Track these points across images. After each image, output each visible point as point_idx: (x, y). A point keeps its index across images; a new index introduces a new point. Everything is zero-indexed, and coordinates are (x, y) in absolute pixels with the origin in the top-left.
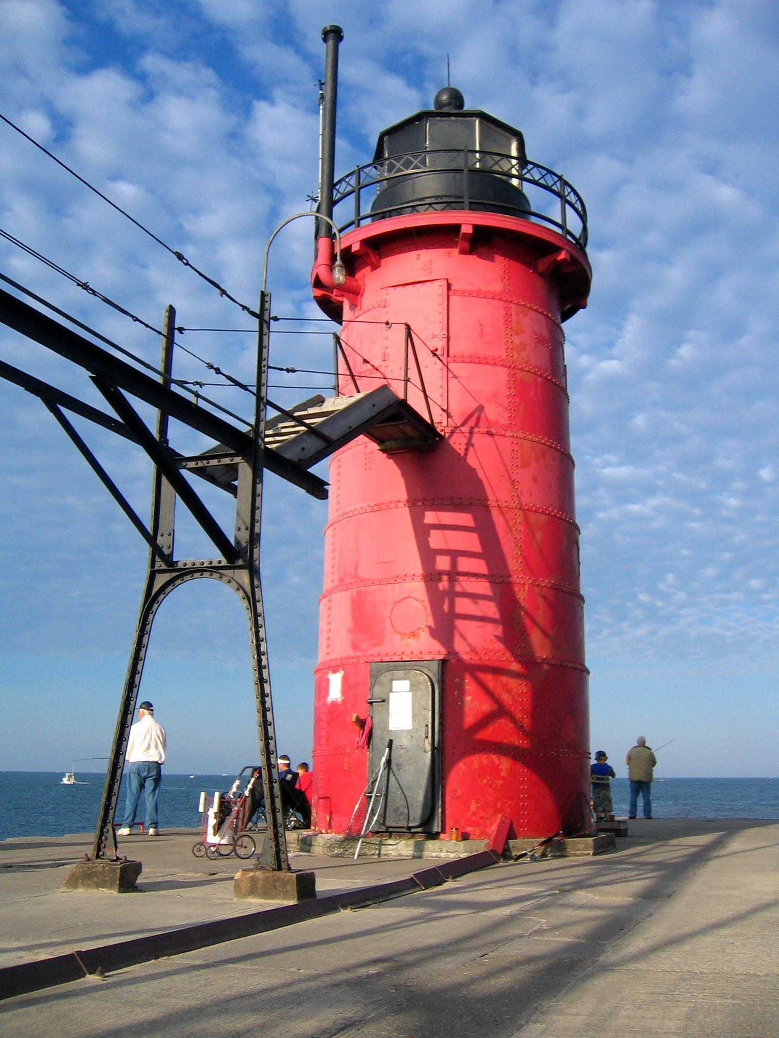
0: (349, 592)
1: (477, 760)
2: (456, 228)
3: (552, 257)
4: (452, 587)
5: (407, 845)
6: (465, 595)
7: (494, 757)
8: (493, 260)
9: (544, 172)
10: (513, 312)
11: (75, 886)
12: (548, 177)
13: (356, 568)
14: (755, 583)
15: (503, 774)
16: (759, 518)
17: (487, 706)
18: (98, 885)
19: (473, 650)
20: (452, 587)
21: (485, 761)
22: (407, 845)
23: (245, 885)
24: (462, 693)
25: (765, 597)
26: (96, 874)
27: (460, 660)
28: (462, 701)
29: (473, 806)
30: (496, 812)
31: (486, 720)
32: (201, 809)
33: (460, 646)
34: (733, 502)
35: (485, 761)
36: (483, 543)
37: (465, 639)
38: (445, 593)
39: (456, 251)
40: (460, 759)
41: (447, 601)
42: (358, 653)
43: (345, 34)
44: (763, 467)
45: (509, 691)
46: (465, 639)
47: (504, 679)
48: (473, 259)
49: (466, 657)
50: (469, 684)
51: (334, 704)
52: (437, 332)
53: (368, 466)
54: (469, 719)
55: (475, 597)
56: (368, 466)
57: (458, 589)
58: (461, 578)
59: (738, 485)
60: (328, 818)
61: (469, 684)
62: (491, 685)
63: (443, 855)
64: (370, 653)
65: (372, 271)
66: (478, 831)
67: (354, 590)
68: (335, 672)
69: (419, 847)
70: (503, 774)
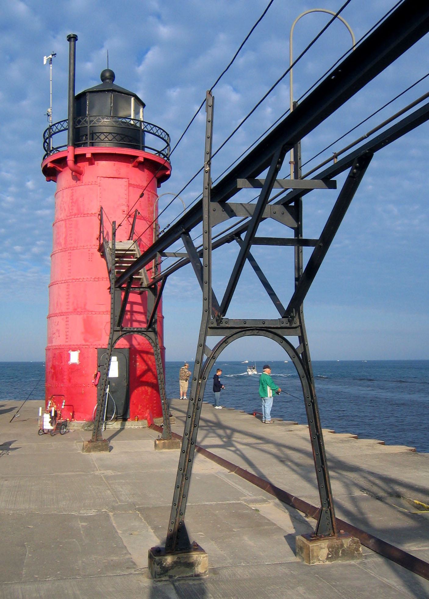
0: (82, 316)
1: (141, 389)
2: (136, 157)
3: (163, 172)
4: (131, 317)
5: (117, 424)
6: (136, 321)
7: (146, 387)
8: (144, 171)
9: (152, 126)
10: (150, 196)
11: (90, 452)
12: (155, 131)
13: (85, 305)
14: (18, 248)
15: (149, 394)
16: (24, 210)
17: (144, 367)
18: (100, 450)
19: (139, 344)
20: (131, 317)
21: (143, 389)
22: (117, 424)
23: (161, 445)
24: (136, 362)
25: (23, 257)
26: (99, 446)
27: (135, 348)
28: (136, 365)
29: (140, 407)
30: (147, 409)
31: (144, 373)
32: (40, 414)
33: (135, 343)
34: (9, 199)
35: (143, 389)
36: (142, 299)
37: (136, 339)
38: (129, 320)
39: (131, 165)
40: (135, 389)
41: (129, 324)
42: (87, 343)
43: (79, 38)
44: (29, 181)
45: (151, 360)
46: (136, 339)
47: (149, 356)
48: (137, 169)
49: (137, 347)
50: (138, 359)
51: (74, 365)
52: (124, 203)
53: (90, 259)
54: (138, 373)
55: (139, 322)
56: (90, 259)
57: (134, 318)
58: (134, 314)
59: (12, 189)
60: (71, 414)
61: (138, 359)
62: (145, 358)
63: (133, 427)
64: (95, 343)
65: (89, 165)
66: (141, 416)
67: (85, 316)
68: (74, 350)
69: (123, 425)
70: (149, 394)
